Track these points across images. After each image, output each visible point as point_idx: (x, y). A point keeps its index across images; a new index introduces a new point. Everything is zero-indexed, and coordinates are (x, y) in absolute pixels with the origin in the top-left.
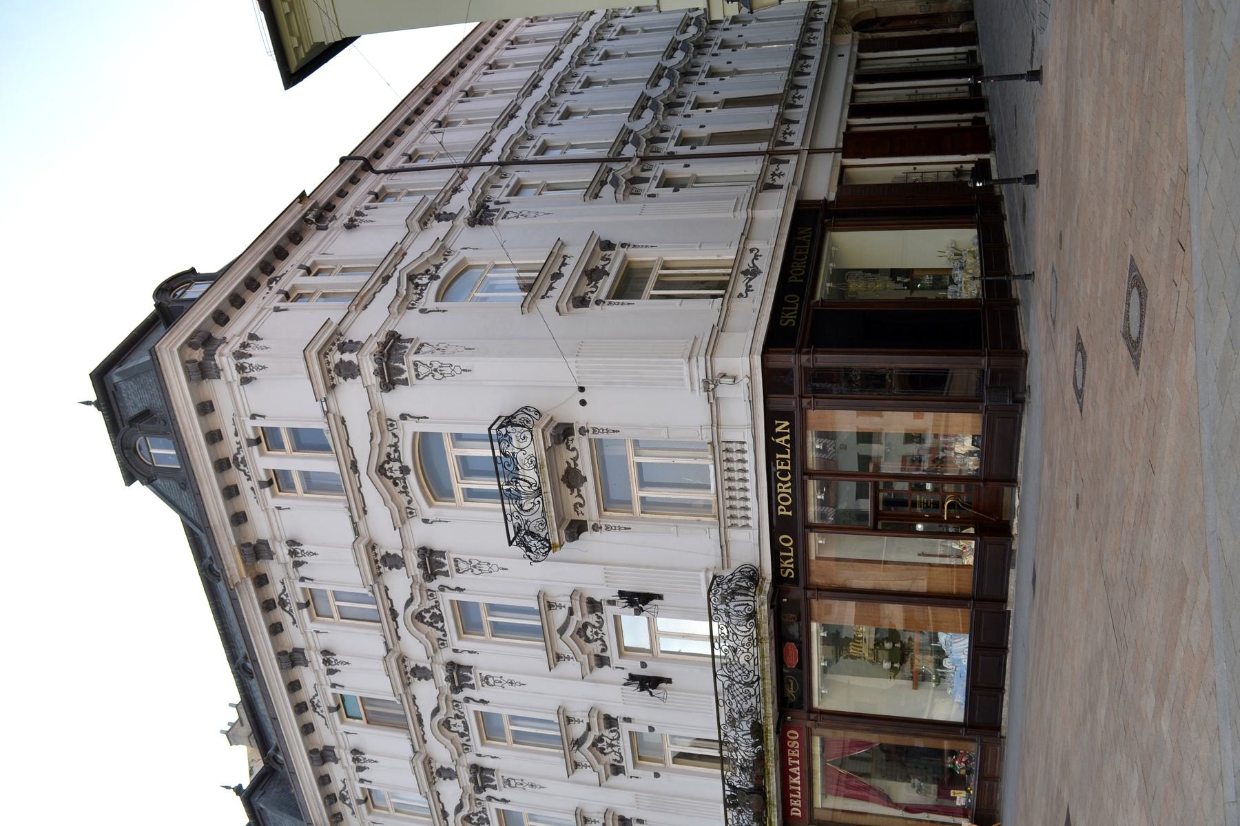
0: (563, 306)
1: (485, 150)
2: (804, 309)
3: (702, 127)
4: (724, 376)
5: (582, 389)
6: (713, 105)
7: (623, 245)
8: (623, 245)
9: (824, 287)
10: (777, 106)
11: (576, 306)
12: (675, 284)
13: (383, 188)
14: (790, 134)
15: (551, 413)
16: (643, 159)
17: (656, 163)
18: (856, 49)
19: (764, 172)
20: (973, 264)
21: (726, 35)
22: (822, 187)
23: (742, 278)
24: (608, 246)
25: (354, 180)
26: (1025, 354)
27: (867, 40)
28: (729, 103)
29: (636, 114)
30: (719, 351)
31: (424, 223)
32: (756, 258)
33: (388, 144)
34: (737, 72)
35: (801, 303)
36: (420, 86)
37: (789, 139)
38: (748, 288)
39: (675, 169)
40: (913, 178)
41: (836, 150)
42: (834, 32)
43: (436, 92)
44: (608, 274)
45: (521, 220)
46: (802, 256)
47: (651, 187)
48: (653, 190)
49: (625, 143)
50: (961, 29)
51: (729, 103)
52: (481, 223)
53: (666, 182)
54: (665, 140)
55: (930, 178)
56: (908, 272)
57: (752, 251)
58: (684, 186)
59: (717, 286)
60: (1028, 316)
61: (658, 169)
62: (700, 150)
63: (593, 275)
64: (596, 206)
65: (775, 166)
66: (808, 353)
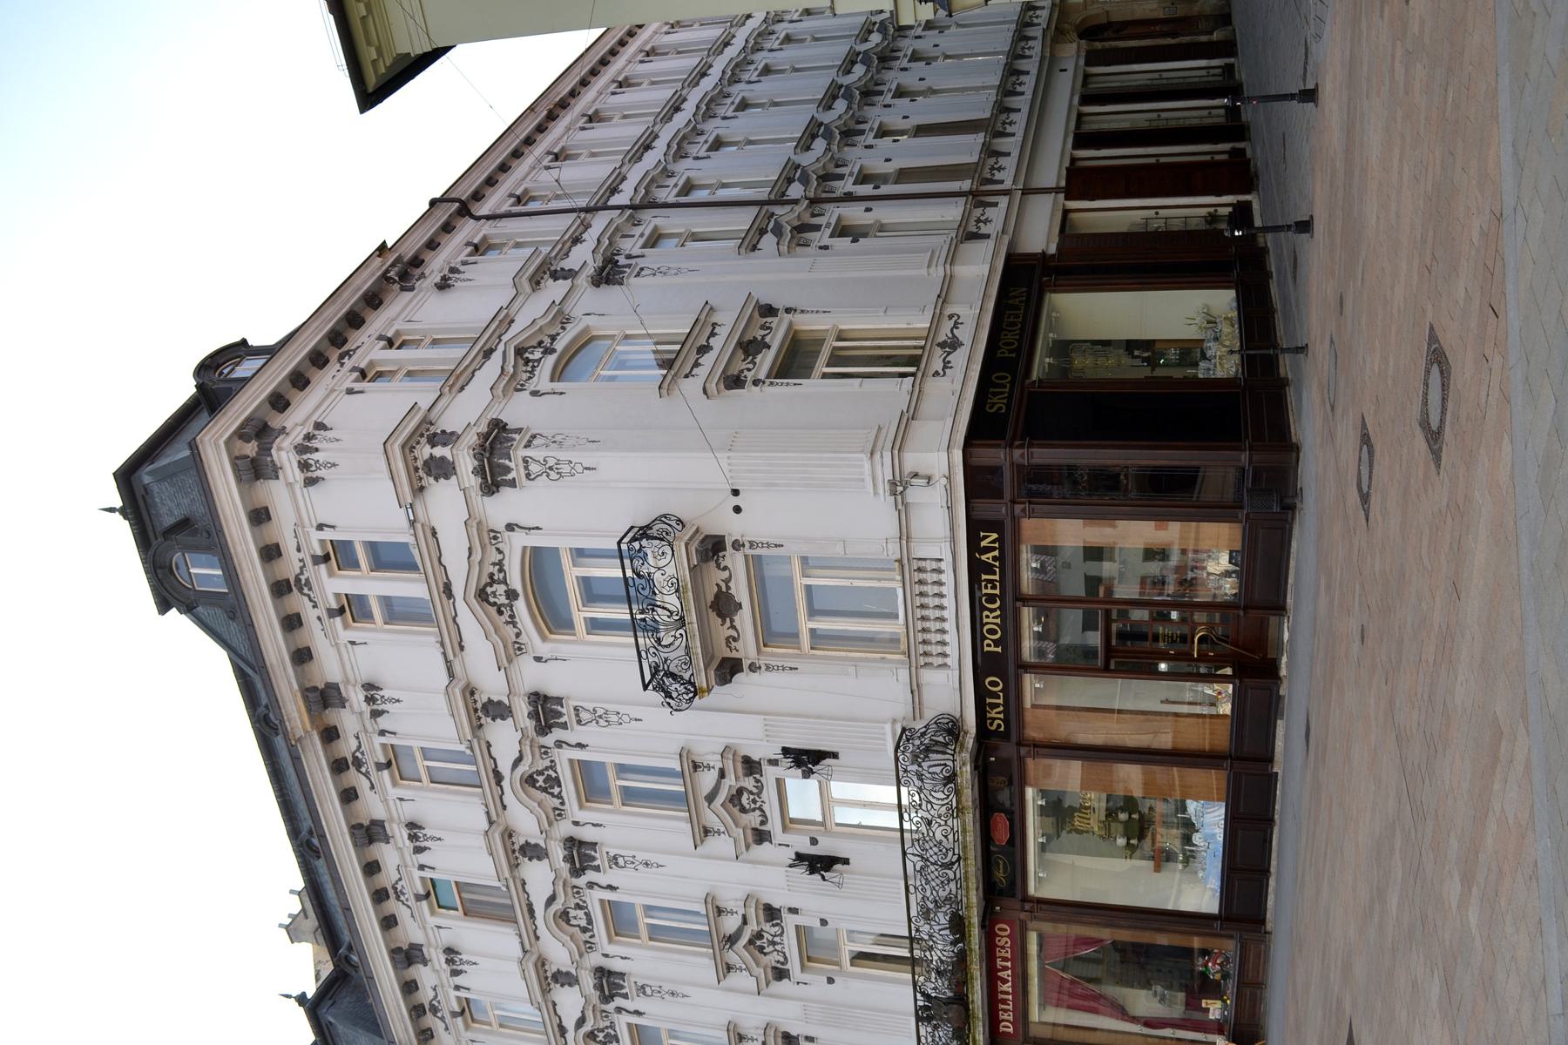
0: (712, 387)
1: (614, 190)
2: (1016, 391)
3: (888, 160)
4: (916, 475)
5: (736, 492)
6: (902, 133)
7: (788, 310)
8: (788, 310)
9: (1041, 364)
10: (982, 135)
11: (728, 387)
12: (853, 360)
13: (485, 238)
14: (999, 169)
15: (697, 523)
16: (813, 201)
17: (830, 207)
18: (1082, 62)
19: (966, 217)
20: (1230, 334)
21: (918, 45)
22: (1040, 236)
23: (939, 351)
24: (768, 311)
25: (447, 228)
26: (1296, 448)
27: (1096, 51)
28: (922, 130)
29: (805, 144)
30: (909, 444)
31: (536, 282)
32: (956, 326)
33: (491, 182)
34: (932, 92)
35: (1013, 383)
36: (531, 108)
37: (998, 176)
38: (946, 365)
39: (854, 214)
40: (1155, 225)
41: (1057, 190)
42: (1055, 41)
43: (552, 116)
44: (769, 347)
45: (659, 279)
46: (1014, 324)
47: (823, 237)
48: (826, 241)
49: (790, 181)
50: (1216, 36)
51: (922, 130)
52: (608, 282)
53: (842, 231)
54: (841, 177)
55: (1176, 225)
56: (1148, 344)
57: (950, 317)
58: (865, 235)
59: (906, 361)
60: (1300, 399)
61: (833, 213)
62: (886, 189)
63: (750, 347)
64: (754, 260)
65: (980, 210)
66: (1021, 446)
